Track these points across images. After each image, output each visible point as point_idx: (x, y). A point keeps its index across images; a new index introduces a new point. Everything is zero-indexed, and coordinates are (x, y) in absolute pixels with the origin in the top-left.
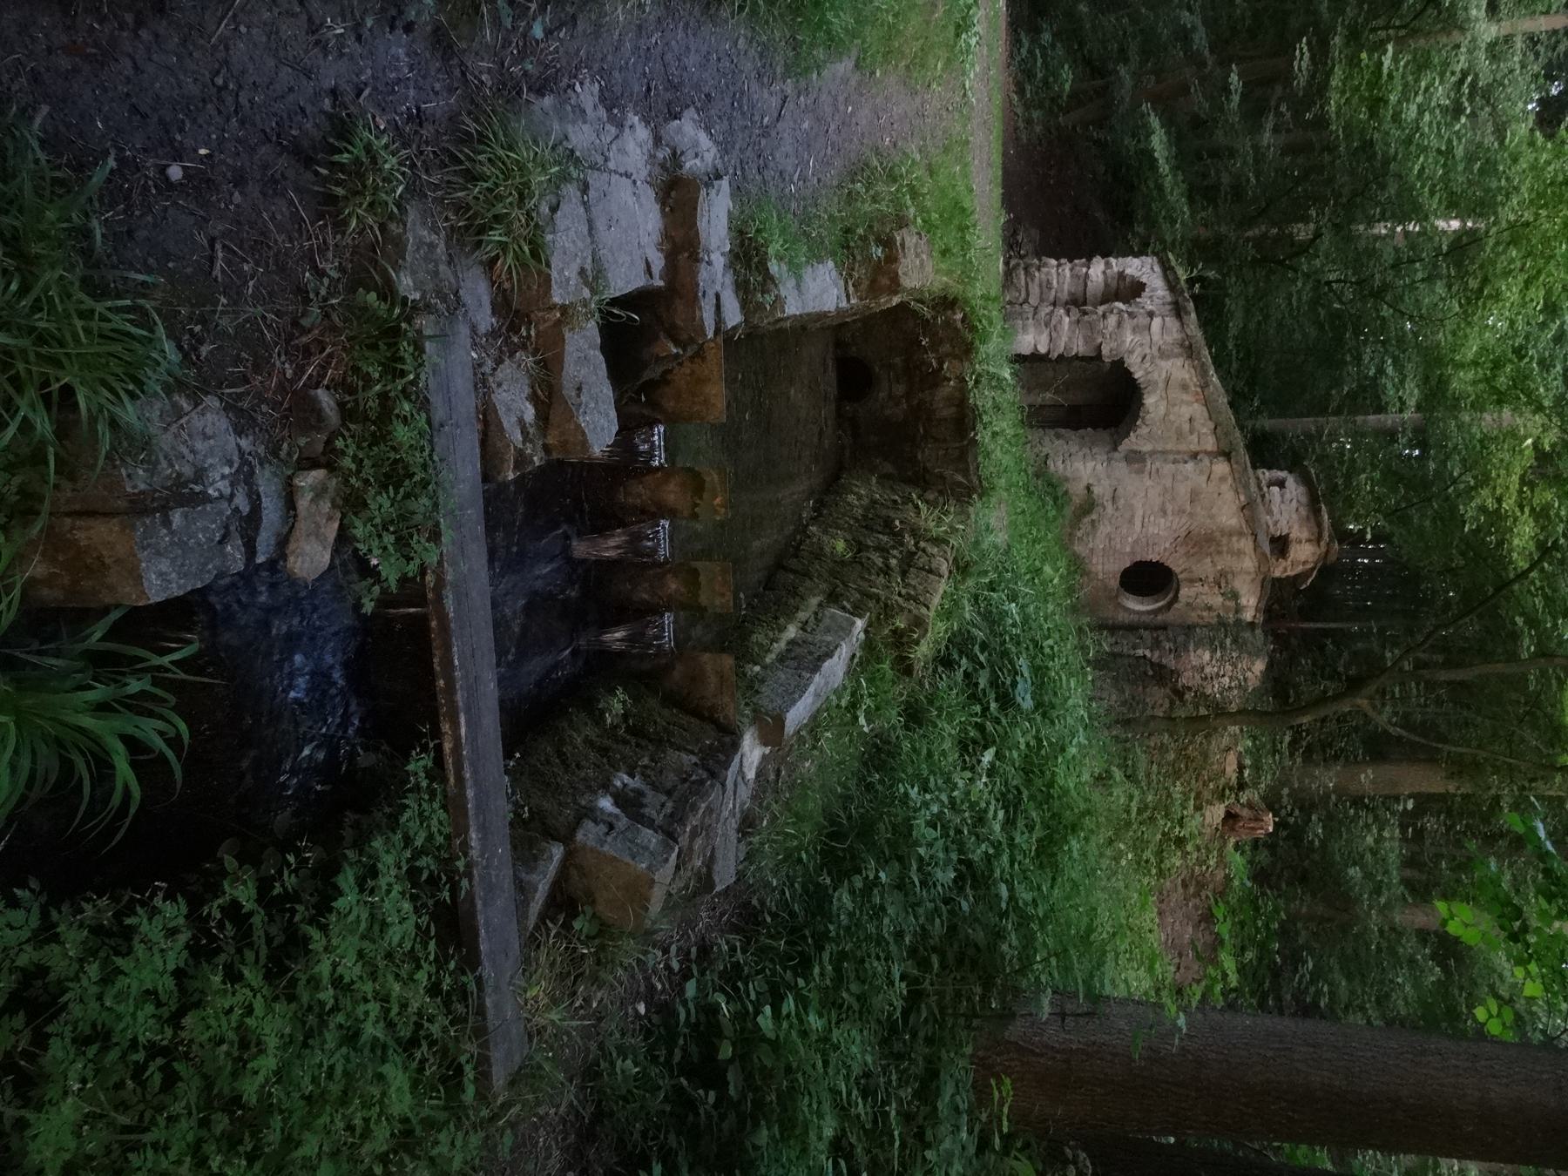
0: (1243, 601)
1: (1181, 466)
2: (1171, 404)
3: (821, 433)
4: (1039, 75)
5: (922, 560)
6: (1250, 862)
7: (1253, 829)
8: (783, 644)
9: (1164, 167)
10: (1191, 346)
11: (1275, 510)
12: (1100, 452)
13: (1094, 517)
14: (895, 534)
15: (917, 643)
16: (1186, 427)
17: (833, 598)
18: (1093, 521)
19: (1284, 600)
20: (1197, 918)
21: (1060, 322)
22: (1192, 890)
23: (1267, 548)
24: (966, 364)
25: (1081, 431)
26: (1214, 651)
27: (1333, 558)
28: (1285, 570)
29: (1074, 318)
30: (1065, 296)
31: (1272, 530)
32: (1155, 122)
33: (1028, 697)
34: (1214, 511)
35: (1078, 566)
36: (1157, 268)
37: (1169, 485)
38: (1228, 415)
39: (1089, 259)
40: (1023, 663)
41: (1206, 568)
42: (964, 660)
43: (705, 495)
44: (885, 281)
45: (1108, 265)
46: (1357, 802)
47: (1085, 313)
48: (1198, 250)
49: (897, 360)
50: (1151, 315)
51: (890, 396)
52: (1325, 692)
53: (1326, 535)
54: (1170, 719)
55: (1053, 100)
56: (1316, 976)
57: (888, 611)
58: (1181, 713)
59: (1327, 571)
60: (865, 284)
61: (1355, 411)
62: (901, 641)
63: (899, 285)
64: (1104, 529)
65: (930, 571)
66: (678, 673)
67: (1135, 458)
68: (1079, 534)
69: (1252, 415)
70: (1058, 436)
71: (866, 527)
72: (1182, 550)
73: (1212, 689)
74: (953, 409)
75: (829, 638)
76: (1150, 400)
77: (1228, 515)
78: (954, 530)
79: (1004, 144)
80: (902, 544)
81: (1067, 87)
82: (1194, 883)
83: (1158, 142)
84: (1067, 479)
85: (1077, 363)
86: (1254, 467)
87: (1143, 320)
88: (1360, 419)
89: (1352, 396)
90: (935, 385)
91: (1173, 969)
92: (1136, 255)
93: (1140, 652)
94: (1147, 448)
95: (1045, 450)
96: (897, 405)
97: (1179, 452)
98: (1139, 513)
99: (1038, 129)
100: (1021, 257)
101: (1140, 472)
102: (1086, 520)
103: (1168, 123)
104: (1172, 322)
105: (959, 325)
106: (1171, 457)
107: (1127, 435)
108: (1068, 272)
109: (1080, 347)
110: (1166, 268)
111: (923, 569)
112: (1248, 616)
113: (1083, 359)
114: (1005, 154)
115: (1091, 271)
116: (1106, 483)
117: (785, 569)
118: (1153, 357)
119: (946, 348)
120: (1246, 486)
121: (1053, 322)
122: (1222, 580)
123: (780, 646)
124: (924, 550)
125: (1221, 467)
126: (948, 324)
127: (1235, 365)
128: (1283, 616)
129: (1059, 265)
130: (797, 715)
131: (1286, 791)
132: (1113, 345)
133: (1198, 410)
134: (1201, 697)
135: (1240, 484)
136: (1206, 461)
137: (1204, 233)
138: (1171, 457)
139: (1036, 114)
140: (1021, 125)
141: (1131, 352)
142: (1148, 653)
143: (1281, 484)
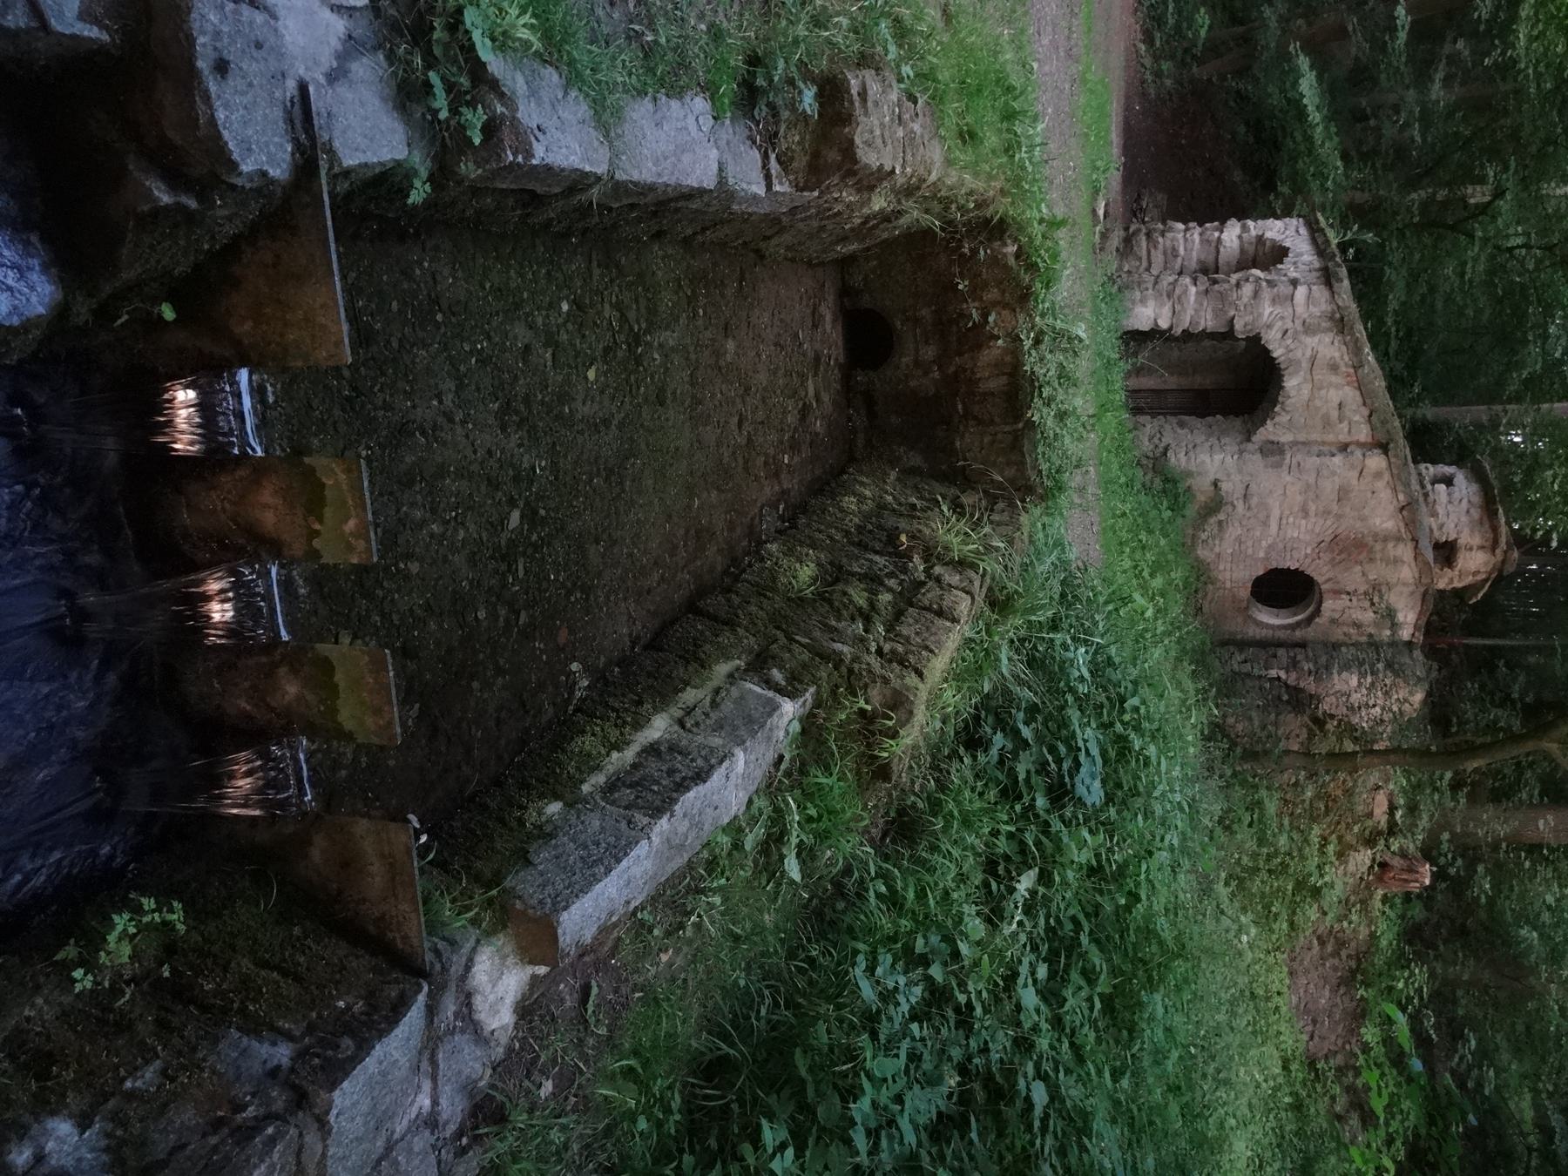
0: (1400, 617)
1: (1327, 460)
2: (1316, 387)
3: (805, 412)
4: (1171, 21)
5: (929, 595)
6: (1402, 917)
7: (1406, 881)
8: (630, 754)
9: (1315, 117)
10: (1342, 319)
11: (1441, 510)
12: (1230, 443)
13: (1221, 516)
14: (900, 555)
15: (894, 735)
16: (1335, 414)
17: (758, 665)
18: (1220, 522)
19: (1449, 616)
20: (1334, 981)
21: (1185, 292)
22: (1329, 948)
23: (1429, 555)
24: (1021, 317)
25: (1210, 419)
26: (1363, 675)
27: (1510, 569)
28: (1451, 580)
29: (1202, 288)
30: (1194, 265)
31: (1436, 534)
32: (1304, 62)
33: (1097, 784)
34: (1366, 512)
35: (1201, 575)
36: (1303, 231)
37: (1312, 480)
38: (1384, 400)
39: (1223, 222)
40: (1089, 736)
41: (1354, 578)
42: (999, 735)
43: (328, 512)
44: (833, 156)
45: (1245, 229)
46: (1534, 849)
47: (1215, 282)
48: (1353, 214)
49: (925, 312)
50: (1294, 283)
51: (917, 363)
52: (1495, 722)
53: (1503, 540)
54: (1307, 754)
55: (1186, 51)
56: (1485, 1054)
57: (853, 681)
58: (1322, 748)
59: (1500, 580)
60: (801, 162)
61: (1537, 400)
62: (869, 727)
63: (856, 162)
64: (1233, 532)
65: (940, 613)
66: (318, 851)
67: (1273, 450)
68: (1204, 536)
69: (1412, 403)
70: (1182, 425)
71: (859, 544)
72: (1326, 557)
73: (1362, 721)
74: (1004, 380)
75: (716, 741)
76: (1291, 383)
77: (1383, 516)
78: (989, 549)
79: (1127, 97)
80: (905, 570)
81: (1203, 33)
82: (1333, 941)
83: (1308, 86)
84: (1189, 474)
85: (1207, 343)
86: (1415, 462)
87: (1284, 289)
88: (1545, 406)
89: (1528, 383)
90: (979, 346)
91: (1305, 1037)
92: (1277, 218)
93: (1273, 673)
94: (1286, 438)
95: (1165, 440)
96: (926, 373)
97: (1324, 443)
98: (1276, 513)
99: (1168, 82)
100: (1144, 222)
101: (1278, 465)
102: (1212, 520)
103: (1322, 66)
104: (1320, 292)
105: (1012, 261)
106: (1315, 449)
107: (1263, 423)
108: (1196, 237)
109: (1208, 321)
110: (1314, 230)
111: (929, 609)
112: (1405, 634)
113: (1213, 336)
114: (1128, 108)
115: (1225, 236)
116: (1237, 478)
117: (699, 612)
118: (1296, 332)
119: (992, 294)
120: (1407, 485)
121: (1177, 292)
122: (1376, 589)
123: (619, 760)
124: (938, 580)
125: (1376, 461)
126: (996, 261)
127: (1394, 344)
128: (1443, 629)
129: (1187, 230)
130: (579, 921)
131: (1446, 836)
132: (1249, 318)
133: (1351, 395)
134: (1349, 730)
135: (1398, 480)
136: (1358, 453)
137: (1360, 197)
138: (1315, 449)
139: (1166, 66)
140: (1149, 77)
141: (1269, 327)
142: (1283, 675)
143: (1448, 481)
